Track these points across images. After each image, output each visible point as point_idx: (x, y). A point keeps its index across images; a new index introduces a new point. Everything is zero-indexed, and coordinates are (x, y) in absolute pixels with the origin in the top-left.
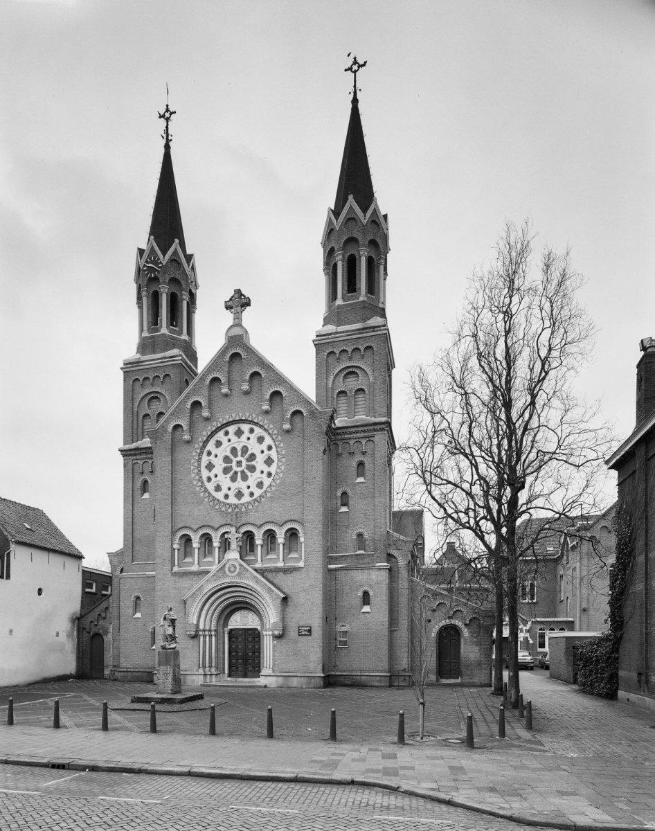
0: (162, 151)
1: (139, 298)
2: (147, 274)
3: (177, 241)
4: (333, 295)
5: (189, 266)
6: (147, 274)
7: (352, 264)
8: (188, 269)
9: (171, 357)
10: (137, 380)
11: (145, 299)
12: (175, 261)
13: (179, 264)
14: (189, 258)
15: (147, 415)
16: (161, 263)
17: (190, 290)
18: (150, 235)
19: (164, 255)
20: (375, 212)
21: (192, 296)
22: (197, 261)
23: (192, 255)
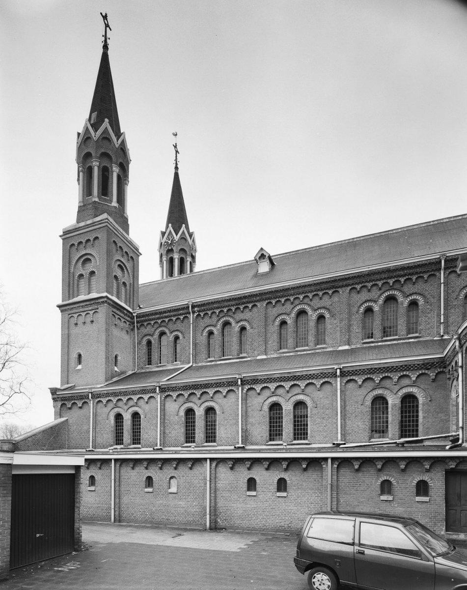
0: (100, 51)
1: (161, 261)
2: (166, 248)
3: (184, 225)
4: (87, 190)
5: (191, 239)
6: (166, 248)
7: (105, 174)
8: (190, 242)
9: (102, 220)
10: (73, 245)
11: (165, 262)
12: (183, 238)
13: (186, 239)
14: (191, 235)
15: (81, 276)
16: (175, 240)
17: (192, 254)
18: (168, 222)
19: (177, 235)
20: (123, 142)
21: (193, 257)
22: (197, 237)
23: (193, 232)
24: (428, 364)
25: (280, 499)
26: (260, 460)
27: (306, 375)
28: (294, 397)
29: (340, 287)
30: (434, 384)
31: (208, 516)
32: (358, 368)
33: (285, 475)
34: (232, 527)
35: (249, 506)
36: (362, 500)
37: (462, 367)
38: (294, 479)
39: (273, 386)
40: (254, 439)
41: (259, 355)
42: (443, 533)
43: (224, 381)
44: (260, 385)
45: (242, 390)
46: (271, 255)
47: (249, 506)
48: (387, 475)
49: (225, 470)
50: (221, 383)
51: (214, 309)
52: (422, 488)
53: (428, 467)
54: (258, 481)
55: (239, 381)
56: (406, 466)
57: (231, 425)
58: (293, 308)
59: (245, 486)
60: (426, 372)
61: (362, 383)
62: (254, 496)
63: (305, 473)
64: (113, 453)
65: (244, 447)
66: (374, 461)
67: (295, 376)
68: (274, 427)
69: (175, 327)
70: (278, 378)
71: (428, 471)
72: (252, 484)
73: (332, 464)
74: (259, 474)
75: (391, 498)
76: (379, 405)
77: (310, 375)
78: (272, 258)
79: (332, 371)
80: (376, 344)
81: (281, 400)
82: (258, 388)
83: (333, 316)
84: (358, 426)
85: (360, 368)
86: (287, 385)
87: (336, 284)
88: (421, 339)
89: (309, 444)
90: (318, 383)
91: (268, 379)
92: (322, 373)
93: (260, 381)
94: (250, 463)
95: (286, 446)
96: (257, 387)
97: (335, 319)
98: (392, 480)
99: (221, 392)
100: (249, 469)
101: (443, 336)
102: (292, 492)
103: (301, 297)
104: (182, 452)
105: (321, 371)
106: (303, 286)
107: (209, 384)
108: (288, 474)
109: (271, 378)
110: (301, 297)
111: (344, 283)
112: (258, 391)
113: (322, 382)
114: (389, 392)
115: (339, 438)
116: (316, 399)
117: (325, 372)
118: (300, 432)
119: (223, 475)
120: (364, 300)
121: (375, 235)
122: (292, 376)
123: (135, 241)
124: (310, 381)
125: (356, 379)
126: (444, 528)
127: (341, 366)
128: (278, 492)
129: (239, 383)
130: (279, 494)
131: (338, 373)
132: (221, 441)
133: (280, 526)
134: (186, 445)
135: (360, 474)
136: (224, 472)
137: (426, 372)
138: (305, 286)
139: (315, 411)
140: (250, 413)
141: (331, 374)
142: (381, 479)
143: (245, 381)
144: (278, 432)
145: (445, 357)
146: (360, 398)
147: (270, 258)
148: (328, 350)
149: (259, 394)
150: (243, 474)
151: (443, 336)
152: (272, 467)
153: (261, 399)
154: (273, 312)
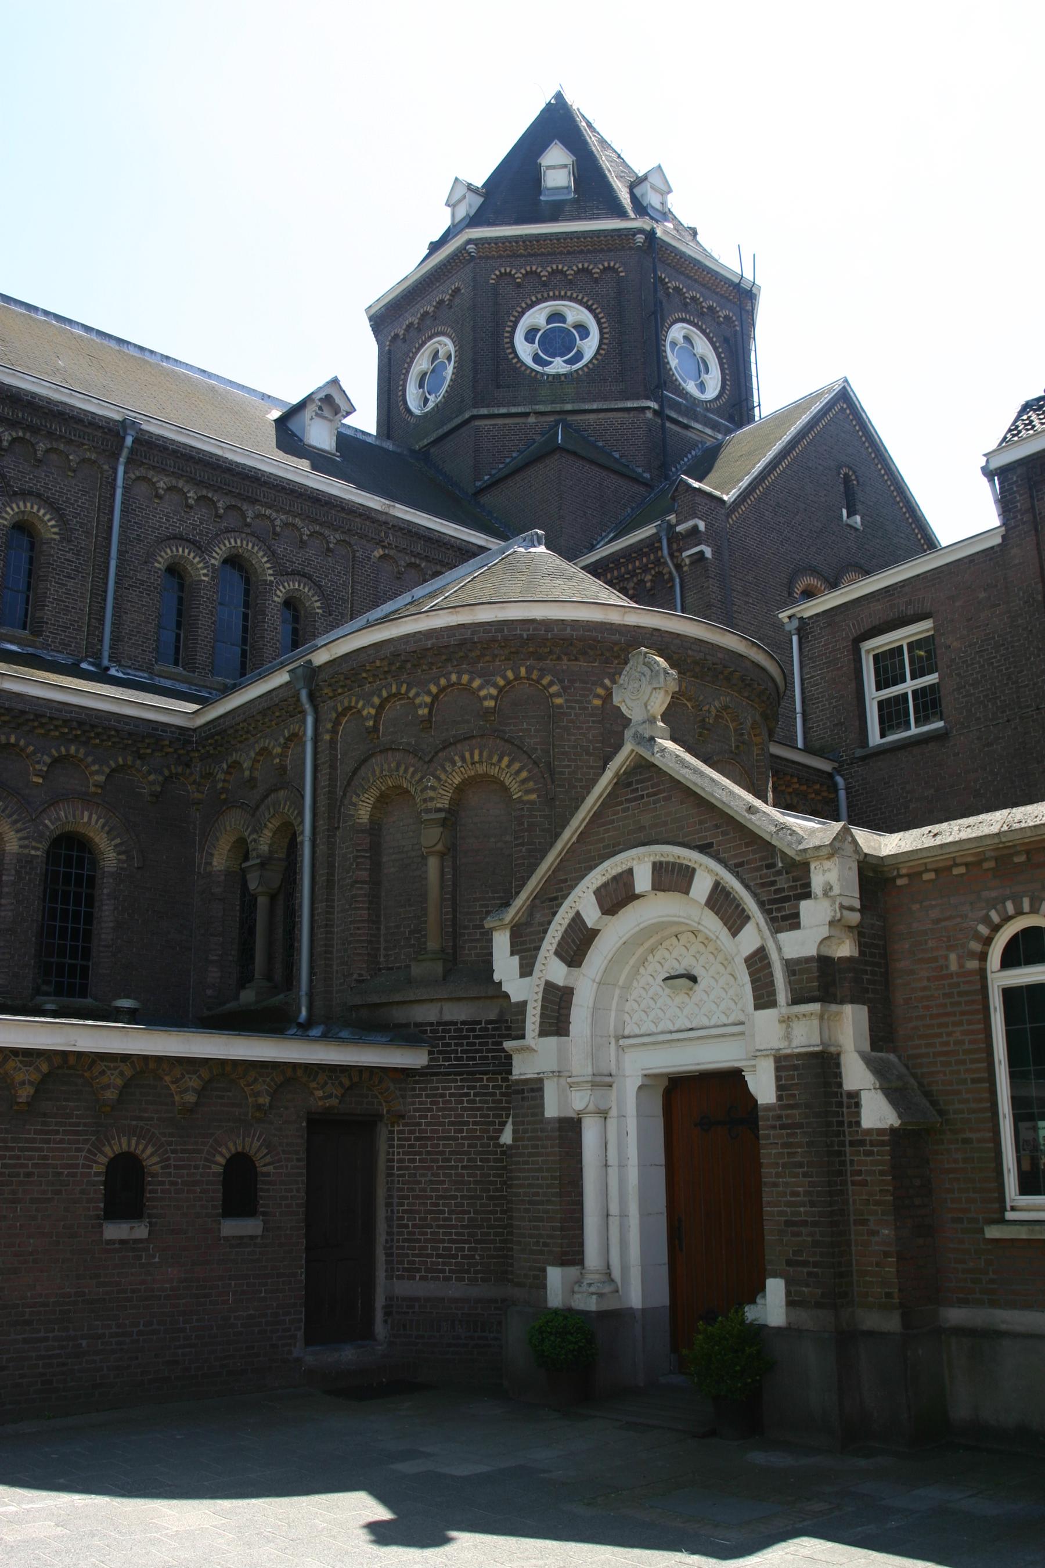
75: (141, 1231)
126: (300, 1334)
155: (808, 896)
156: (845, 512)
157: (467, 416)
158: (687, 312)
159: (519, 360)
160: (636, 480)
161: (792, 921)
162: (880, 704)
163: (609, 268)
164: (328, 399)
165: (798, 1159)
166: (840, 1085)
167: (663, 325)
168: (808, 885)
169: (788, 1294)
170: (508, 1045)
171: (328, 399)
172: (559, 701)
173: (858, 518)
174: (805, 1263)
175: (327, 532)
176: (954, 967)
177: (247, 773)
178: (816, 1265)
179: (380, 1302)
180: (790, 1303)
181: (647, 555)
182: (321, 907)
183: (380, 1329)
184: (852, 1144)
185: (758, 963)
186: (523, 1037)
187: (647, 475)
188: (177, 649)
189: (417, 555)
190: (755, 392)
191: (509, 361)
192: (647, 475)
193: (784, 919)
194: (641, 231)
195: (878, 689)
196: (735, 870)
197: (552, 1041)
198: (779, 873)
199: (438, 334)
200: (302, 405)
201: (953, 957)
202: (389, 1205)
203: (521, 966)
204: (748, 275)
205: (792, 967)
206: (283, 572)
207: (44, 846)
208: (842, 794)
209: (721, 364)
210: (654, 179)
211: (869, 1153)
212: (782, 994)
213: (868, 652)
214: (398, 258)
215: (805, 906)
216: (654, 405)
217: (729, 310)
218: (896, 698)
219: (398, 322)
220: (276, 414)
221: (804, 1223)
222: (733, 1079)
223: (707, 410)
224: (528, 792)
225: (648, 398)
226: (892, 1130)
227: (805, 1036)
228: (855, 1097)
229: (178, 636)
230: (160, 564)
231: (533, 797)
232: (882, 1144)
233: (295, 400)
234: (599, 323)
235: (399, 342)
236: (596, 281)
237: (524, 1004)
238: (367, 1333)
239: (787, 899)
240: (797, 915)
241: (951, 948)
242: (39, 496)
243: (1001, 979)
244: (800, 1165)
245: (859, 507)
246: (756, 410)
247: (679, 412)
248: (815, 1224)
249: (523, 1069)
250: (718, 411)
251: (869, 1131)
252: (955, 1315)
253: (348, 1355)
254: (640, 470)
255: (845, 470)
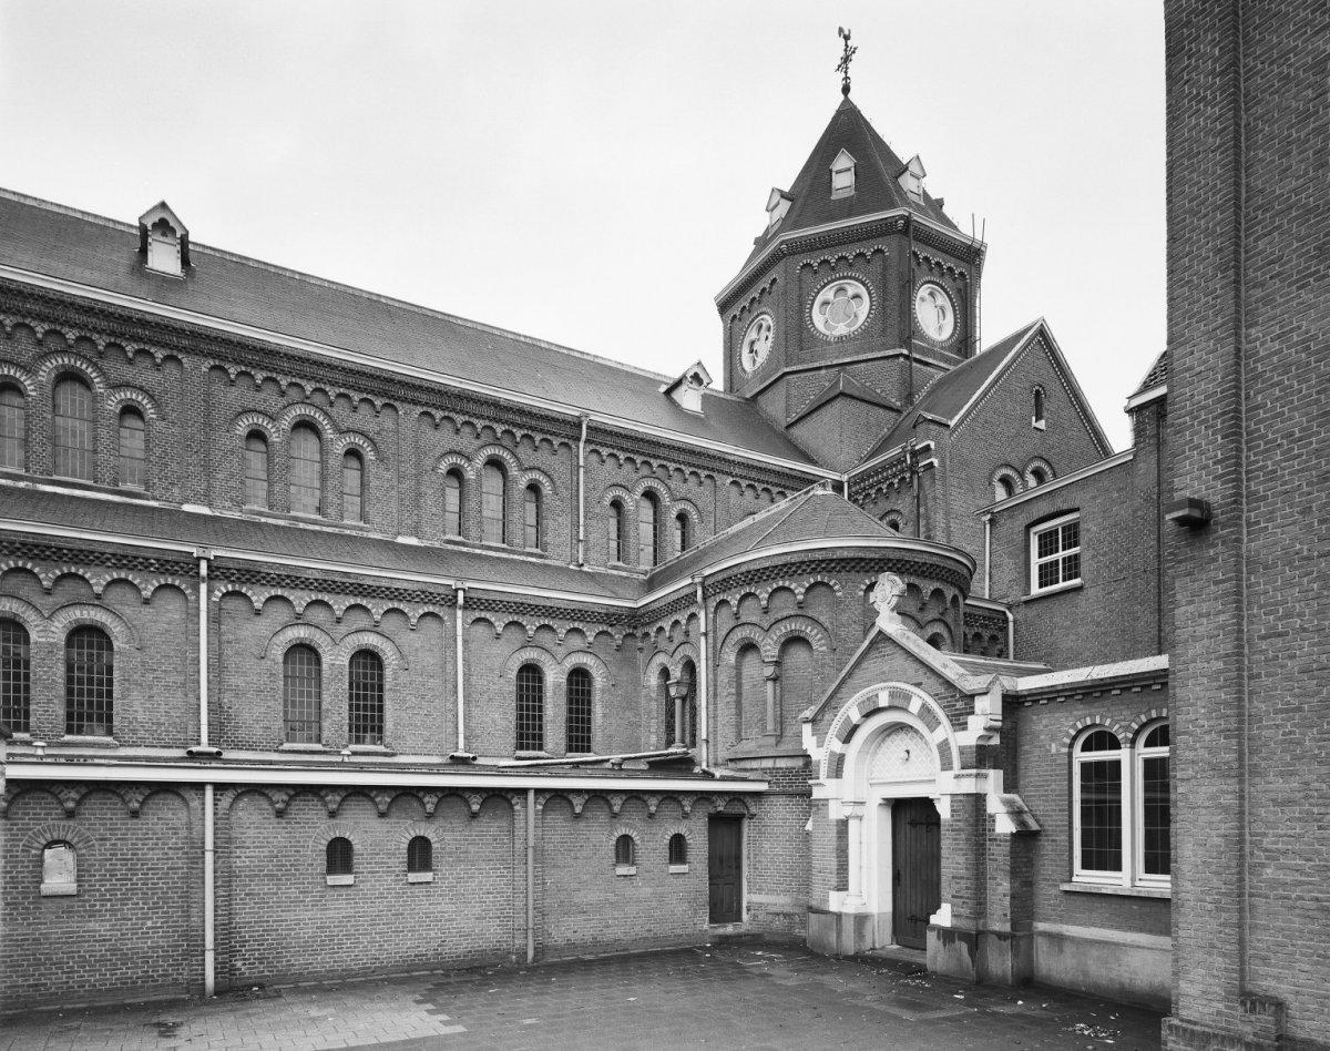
24: (614, 614)
25: (416, 889)
26: (112, 787)
27: (388, 589)
28: (354, 637)
29: (404, 400)
30: (618, 655)
31: (209, 957)
32: (498, 597)
33: (429, 831)
34: (282, 978)
35: (330, 913)
36: (585, 878)
37: (706, 634)
38: (448, 837)
39: (300, 599)
40: (242, 733)
41: (187, 501)
42: (706, 927)
43: (148, 555)
44: (263, 589)
45: (210, 592)
46: (191, 238)
47: (330, 913)
48: (627, 825)
49: (256, 818)
50: (136, 558)
51: (24, 317)
52: (678, 849)
53: (430, 808)
54: (357, 847)
55: (204, 565)
56: (437, 806)
57: (167, 687)
58: (285, 407)
59: (322, 860)
60: (610, 630)
61: (104, 591)
62: (428, 883)
63: (474, 823)
64: (500, 768)
65: (219, 753)
66: (570, 797)
67: (361, 585)
68: (373, 706)
69: (128, 373)
70: (316, 580)
71: (430, 817)
72: (340, 855)
73: (536, 799)
74: (360, 828)
75: (633, 870)
76: (365, 667)
77: (397, 589)
78: (191, 247)
79: (447, 593)
80: (471, 550)
81: (319, 640)
82: (258, 596)
83: (381, 459)
84: (494, 721)
85: (503, 599)
86: (340, 603)
87: (393, 389)
88: (547, 562)
89: (393, 755)
90: (414, 611)
91: (288, 577)
92: (423, 592)
93: (264, 578)
94: (338, 799)
95: (348, 756)
96: (254, 594)
97: (388, 470)
98: (634, 835)
99: (554, 630)
100: (332, 815)
101: (582, 565)
102: (445, 872)
103: (71, 335)
104: (97, 761)
105: (424, 587)
106: (315, 362)
107: (92, 552)
108: (434, 827)
109: (298, 578)
110: (309, 387)
111: (410, 394)
112: (147, 594)
113: (421, 612)
114: (549, 656)
115: (461, 745)
116: (405, 650)
117: (430, 590)
118: (367, 720)
119: (251, 832)
120: (447, 447)
121: (572, 353)
122: (352, 584)
123: (1076, 375)
124: (396, 605)
125: (493, 620)
126: (707, 918)
127: (467, 585)
128: (409, 871)
129: (204, 570)
130: (412, 877)
131: (461, 600)
132: (134, 731)
133: (416, 956)
134: (68, 738)
135: (582, 825)
136: (252, 819)
137: (610, 630)
138: (319, 364)
139: (404, 678)
140: (232, 661)
141: (443, 599)
142: (617, 834)
143: (218, 568)
144: (361, 723)
145: (638, 608)
146: (497, 663)
147: (184, 242)
148: (371, 535)
149: (258, 613)
150: (316, 830)
151: (582, 565)
152: (394, 810)
153: (262, 626)
154: (237, 396)
155: (973, 713)
156: (1034, 418)
157: (780, 374)
158: (932, 275)
159: (815, 329)
160: (890, 409)
161: (963, 726)
162: (1041, 567)
163: (879, 251)
164: (696, 377)
165: (960, 847)
166: (985, 810)
167: (914, 289)
168: (973, 708)
169: (953, 911)
170: (810, 782)
171: (696, 377)
172: (839, 594)
173: (1043, 422)
174: (961, 897)
175: (699, 471)
176: (1054, 751)
177: (668, 633)
178: (968, 898)
179: (744, 904)
180: (954, 916)
181: (895, 465)
182: (711, 707)
183: (745, 916)
184: (990, 840)
185: (944, 748)
186: (818, 778)
187: (898, 404)
188: (619, 551)
189: (753, 479)
190: (978, 330)
191: (809, 330)
192: (898, 404)
193: (959, 723)
194: (902, 217)
195: (1040, 556)
196: (935, 696)
197: (834, 781)
198: (957, 701)
199: (762, 313)
200: (678, 383)
201: (1053, 745)
202: (749, 858)
203: (818, 742)
204: (978, 237)
205: (962, 751)
206: (675, 500)
207: (565, 677)
208: (1011, 625)
209: (954, 310)
210: (914, 168)
211: (998, 845)
212: (956, 763)
213: (1035, 533)
214: (731, 262)
215: (971, 719)
216: (905, 352)
217: (960, 264)
218: (1051, 563)
219: (735, 304)
220: (663, 388)
221: (962, 878)
222: (927, 804)
223: (942, 348)
224: (821, 646)
225: (901, 347)
226: (1012, 834)
227: (969, 786)
228: (992, 818)
229: (618, 543)
230: (607, 502)
231: (824, 648)
232: (1006, 841)
233: (677, 376)
234: (869, 294)
235: (736, 321)
236: (868, 261)
237: (819, 762)
238: (738, 918)
239: (961, 714)
240: (966, 723)
241: (1053, 740)
242: (539, 469)
243: (1080, 757)
244: (962, 849)
245: (1045, 414)
246: (978, 343)
247: (923, 354)
248: (968, 879)
249: (817, 794)
250: (950, 348)
251: (999, 835)
252: (1041, 926)
253: (730, 929)
254: (893, 400)
255: (1037, 388)
